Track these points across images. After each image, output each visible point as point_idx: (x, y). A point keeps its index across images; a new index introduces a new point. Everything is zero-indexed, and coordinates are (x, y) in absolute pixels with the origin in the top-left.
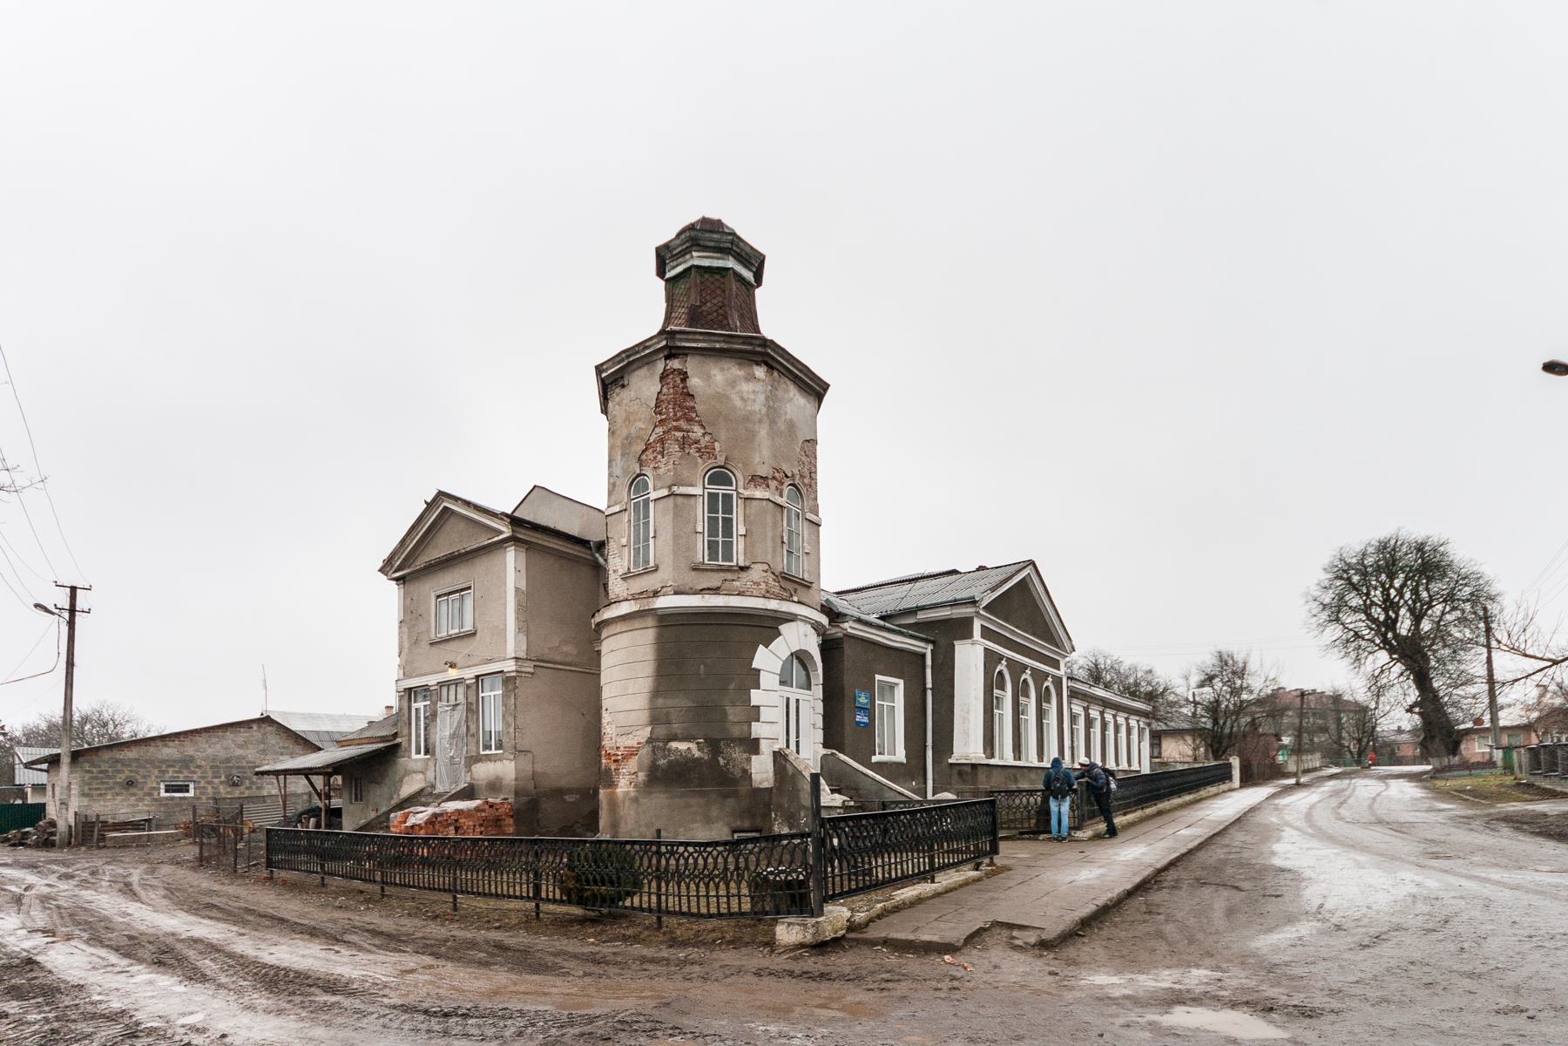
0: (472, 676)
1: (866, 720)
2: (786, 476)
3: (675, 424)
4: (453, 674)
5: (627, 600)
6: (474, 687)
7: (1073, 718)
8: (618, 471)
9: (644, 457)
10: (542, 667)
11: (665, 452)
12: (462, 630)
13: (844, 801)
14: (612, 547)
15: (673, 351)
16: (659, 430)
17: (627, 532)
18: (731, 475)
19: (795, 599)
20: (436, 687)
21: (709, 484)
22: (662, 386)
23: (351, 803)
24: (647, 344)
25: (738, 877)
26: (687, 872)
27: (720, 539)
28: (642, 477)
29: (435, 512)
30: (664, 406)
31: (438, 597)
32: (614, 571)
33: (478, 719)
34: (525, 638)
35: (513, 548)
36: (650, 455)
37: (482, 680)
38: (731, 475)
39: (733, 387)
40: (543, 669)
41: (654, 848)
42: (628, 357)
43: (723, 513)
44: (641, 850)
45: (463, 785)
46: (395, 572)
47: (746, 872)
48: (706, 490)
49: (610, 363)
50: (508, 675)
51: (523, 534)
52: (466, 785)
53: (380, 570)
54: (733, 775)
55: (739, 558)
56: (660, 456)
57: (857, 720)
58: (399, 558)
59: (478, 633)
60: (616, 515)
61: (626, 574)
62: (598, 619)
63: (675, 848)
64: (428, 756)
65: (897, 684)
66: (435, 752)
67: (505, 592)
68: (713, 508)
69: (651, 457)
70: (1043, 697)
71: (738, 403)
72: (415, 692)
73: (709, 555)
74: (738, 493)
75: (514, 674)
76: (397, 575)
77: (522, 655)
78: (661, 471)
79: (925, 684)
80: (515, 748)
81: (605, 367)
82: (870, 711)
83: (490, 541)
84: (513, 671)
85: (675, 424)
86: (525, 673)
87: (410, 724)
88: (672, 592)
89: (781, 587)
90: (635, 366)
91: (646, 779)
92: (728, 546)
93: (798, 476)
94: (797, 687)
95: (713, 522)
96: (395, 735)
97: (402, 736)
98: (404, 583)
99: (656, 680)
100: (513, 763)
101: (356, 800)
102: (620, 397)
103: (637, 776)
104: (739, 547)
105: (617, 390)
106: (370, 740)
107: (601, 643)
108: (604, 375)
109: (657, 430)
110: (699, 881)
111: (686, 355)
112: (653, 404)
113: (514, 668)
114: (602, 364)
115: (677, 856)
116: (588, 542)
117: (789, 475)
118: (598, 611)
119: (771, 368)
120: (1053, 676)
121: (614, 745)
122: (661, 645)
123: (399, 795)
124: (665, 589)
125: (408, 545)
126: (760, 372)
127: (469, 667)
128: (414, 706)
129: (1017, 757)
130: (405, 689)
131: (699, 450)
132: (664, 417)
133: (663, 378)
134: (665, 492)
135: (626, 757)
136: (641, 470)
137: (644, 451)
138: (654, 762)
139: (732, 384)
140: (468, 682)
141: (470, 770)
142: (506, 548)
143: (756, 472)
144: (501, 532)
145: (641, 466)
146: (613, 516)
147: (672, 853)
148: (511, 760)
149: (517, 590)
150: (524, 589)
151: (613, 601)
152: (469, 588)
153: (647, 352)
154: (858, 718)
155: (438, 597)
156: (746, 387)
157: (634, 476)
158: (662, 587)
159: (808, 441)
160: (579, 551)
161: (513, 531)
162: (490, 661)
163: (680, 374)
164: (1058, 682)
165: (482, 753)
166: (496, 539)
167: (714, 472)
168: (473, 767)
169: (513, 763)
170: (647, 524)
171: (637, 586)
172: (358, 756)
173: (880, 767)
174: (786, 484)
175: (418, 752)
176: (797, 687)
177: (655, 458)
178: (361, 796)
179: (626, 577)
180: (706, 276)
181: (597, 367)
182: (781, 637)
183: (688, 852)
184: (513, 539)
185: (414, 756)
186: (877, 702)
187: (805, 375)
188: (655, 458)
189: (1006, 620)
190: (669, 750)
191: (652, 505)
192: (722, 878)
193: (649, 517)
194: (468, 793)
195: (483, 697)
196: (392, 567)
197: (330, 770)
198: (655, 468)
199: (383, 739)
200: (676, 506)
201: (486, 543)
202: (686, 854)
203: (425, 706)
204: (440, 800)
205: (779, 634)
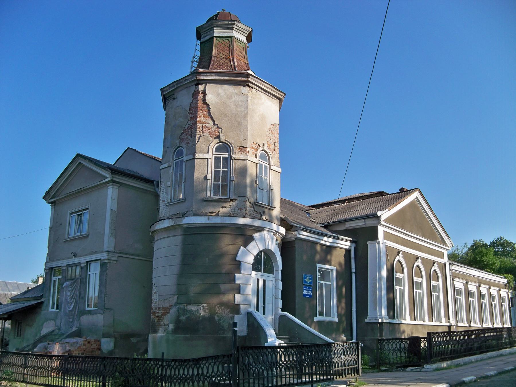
0: (85, 261)
1: (310, 293)
2: (259, 146)
4: (75, 260)
5: (168, 219)
6: (85, 268)
7: (457, 292)
9: (182, 137)
10: (122, 257)
11: (192, 135)
12: (82, 234)
13: (280, 344)
14: (162, 186)
17: (171, 179)
21: (215, 152)
22: (193, 99)
23: (14, 338)
24: (186, 78)
25: (198, 379)
26: (175, 376)
28: (180, 148)
31: (71, 213)
32: (163, 201)
33: (86, 288)
34: (114, 239)
35: (112, 186)
36: (185, 136)
37: (90, 264)
39: (230, 99)
40: (123, 258)
41: (160, 363)
43: (222, 168)
44: (154, 364)
45: (74, 329)
46: (51, 199)
47: (202, 377)
48: (214, 156)
49: (168, 88)
50: (103, 262)
52: (77, 329)
53: (43, 198)
54: (223, 327)
56: (190, 137)
57: (304, 293)
58: (54, 191)
59: (90, 237)
60: (166, 169)
61: (169, 203)
62: (152, 229)
63: (170, 363)
64: (58, 310)
66: (61, 307)
69: (186, 137)
72: (55, 270)
75: (107, 261)
76: (51, 200)
77: (112, 249)
79: (351, 269)
80: (104, 306)
81: (165, 89)
82: (313, 287)
83: (100, 183)
84: (106, 259)
86: (113, 260)
87: (50, 290)
88: (192, 215)
89: (255, 211)
90: (180, 89)
91: (174, 328)
93: (267, 145)
94: (264, 272)
96: (42, 296)
98: (55, 205)
100: (102, 316)
101: (17, 337)
102: (172, 103)
103: (168, 326)
105: (171, 101)
106: (30, 299)
107: (155, 242)
108: (165, 93)
112: (188, 109)
113: (107, 257)
117: (261, 145)
118: (153, 224)
120: (439, 263)
121: (157, 307)
122: (185, 246)
123: (41, 334)
124: (188, 213)
125: (60, 183)
127: (83, 256)
128: (54, 278)
129: (413, 318)
131: (210, 133)
132: (193, 116)
135: (164, 314)
136: (180, 144)
137: (182, 134)
138: (178, 317)
140: (82, 265)
141: (79, 320)
142: (108, 186)
144: (106, 178)
146: (165, 169)
147: (169, 366)
148: (102, 314)
149: (112, 210)
150: (116, 210)
151: (161, 219)
152: (87, 209)
153: (186, 82)
154: (305, 292)
155: (71, 213)
157: (176, 147)
158: (187, 211)
160: (147, 187)
161: (112, 177)
162: (94, 253)
165: (87, 309)
166: (104, 181)
168: (81, 318)
169: (102, 316)
170: (181, 175)
171: (174, 210)
172: (21, 308)
173: (321, 326)
174: (259, 150)
175: (53, 307)
176: (264, 272)
177: (187, 138)
178: (20, 334)
179: (170, 204)
181: (161, 89)
185: (51, 310)
186: (318, 281)
188: (187, 138)
189: (402, 228)
190: (187, 311)
191: (184, 164)
192: (191, 379)
193: (183, 171)
194: (78, 334)
195: (89, 275)
196: (50, 196)
197: (6, 316)
199: (35, 298)
201: (98, 183)
202: (175, 366)
203: (59, 279)
204: (62, 338)
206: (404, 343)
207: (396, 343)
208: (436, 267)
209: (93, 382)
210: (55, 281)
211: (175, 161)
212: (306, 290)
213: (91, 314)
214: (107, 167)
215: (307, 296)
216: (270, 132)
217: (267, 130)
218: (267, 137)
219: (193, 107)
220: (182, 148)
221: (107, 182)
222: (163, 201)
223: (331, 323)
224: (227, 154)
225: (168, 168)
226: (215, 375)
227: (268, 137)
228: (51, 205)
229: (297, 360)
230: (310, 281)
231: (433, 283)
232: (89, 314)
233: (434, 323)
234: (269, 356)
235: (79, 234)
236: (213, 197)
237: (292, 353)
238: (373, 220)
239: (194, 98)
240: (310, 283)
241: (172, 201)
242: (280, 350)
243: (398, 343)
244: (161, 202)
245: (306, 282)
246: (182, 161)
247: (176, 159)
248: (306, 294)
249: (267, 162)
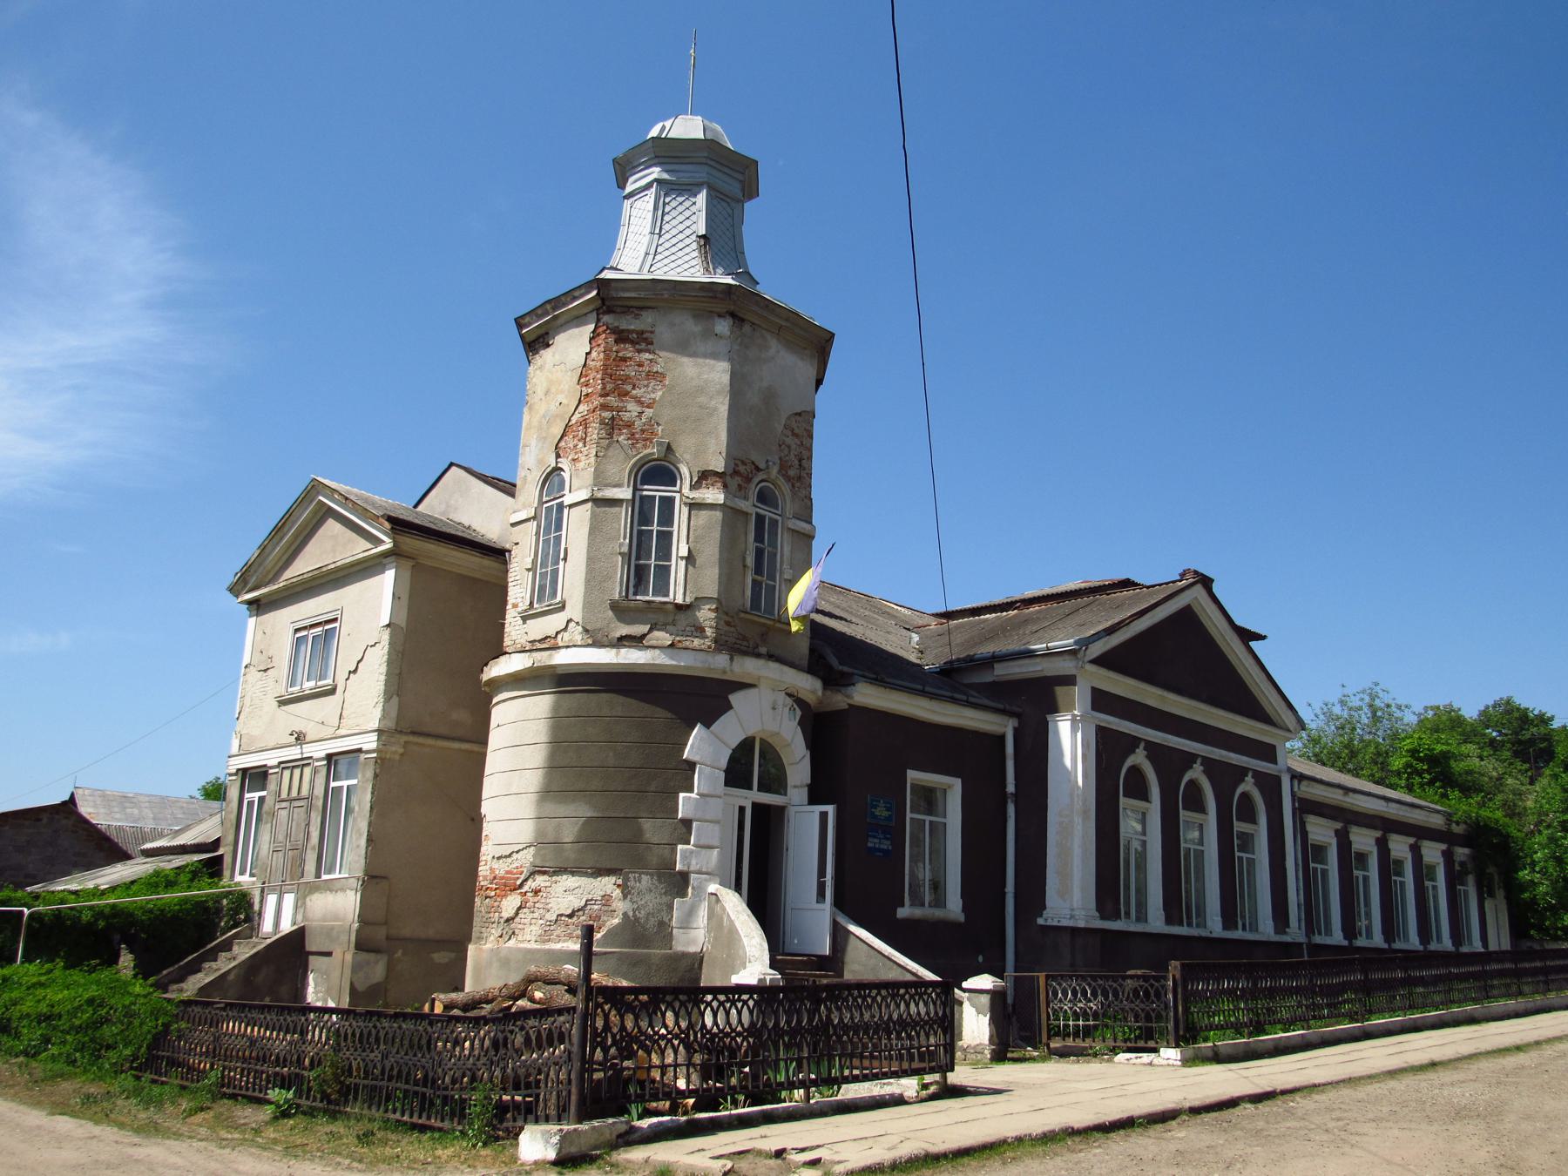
0: (322, 754)
1: (886, 845)
7: (1312, 853)
9: (562, 444)
11: (588, 439)
19: (763, 650)
20: (276, 770)
28: (558, 472)
29: (306, 509)
30: (591, 376)
36: (569, 441)
37: (336, 761)
48: (677, 488)
51: (412, 543)
56: (581, 444)
57: (870, 845)
65: (950, 787)
70: (1233, 812)
74: (682, 495)
78: (581, 465)
81: (527, 319)
92: (663, 572)
97: (226, 845)
99: (547, 772)
114: (522, 317)
130: (238, 770)
136: (557, 463)
143: (708, 465)
145: (558, 456)
150: (404, 625)
159: (799, 414)
164: (1270, 786)
167: (643, 474)
168: (308, 899)
177: (575, 446)
182: (730, 713)
184: (393, 553)
186: (909, 815)
188: (575, 446)
191: (566, 511)
198: (574, 460)
205: (729, 707)
208: (1248, 785)
210: (251, 803)
211: (545, 505)
212: (874, 837)
213: (331, 891)
214: (382, 516)
215: (878, 854)
216: (790, 433)
217: (780, 428)
218: (780, 446)
221: (386, 554)
222: (515, 606)
223: (944, 927)
224: (645, 493)
227: (783, 446)
228: (248, 609)
229: (752, 1024)
230: (886, 814)
231: (1239, 826)
232: (326, 890)
233: (1238, 934)
234: (734, 1011)
235: (312, 684)
237: (932, 998)
238: (1064, 660)
239: (594, 344)
240: (889, 818)
242: (715, 998)
244: (509, 606)
245: (875, 817)
246: (561, 507)
247: (548, 499)
248: (875, 848)
249: (777, 509)
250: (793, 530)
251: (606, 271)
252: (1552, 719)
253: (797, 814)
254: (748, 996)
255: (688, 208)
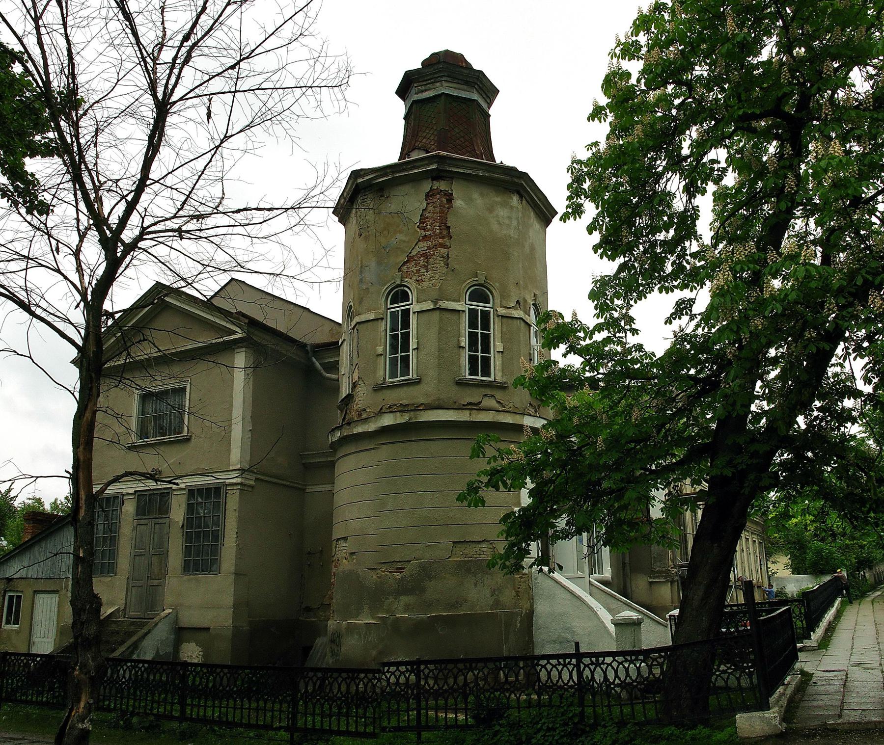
3: (441, 241)
8: (370, 275)
15: (26, 57)
16: (424, 245)
17: (383, 341)
18: (489, 293)
22: (428, 204)
27: (480, 354)
35: (244, 349)
38: (489, 293)
42: (393, 173)
55: (496, 374)
67: (232, 397)
68: (473, 324)
69: (414, 269)
71: (495, 227)
73: (470, 369)
85: (441, 241)
95: (473, 337)
104: (496, 362)
108: (360, 180)
109: (421, 244)
110: (325, 702)
111: (452, 178)
115: (307, 679)
116: (305, 345)
119: (521, 197)
126: (515, 199)
132: (428, 233)
133: (428, 196)
134: (429, 305)
136: (401, 281)
137: (405, 263)
139: (491, 210)
144: (234, 332)
147: (598, 664)
156: (502, 212)
163: (445, 194)
166: (226, 338)
180: (455, 104)
183: (428, 669)
187: (543, 203)
200: (441, 320)
206: (604, 667)
207: (340, 680)
209: (172, 704)
219: (427, 218)
220: (406, 289)
225: (376, 322)
226: (644, 681)
236: (470, 377)
241: (387, 380)
243: (587, 669)
250: (502, 316)
251: (131, 120)
252: (599, 332)
253: (157, 526)
254: (546, 661)
255: (238, 78)
